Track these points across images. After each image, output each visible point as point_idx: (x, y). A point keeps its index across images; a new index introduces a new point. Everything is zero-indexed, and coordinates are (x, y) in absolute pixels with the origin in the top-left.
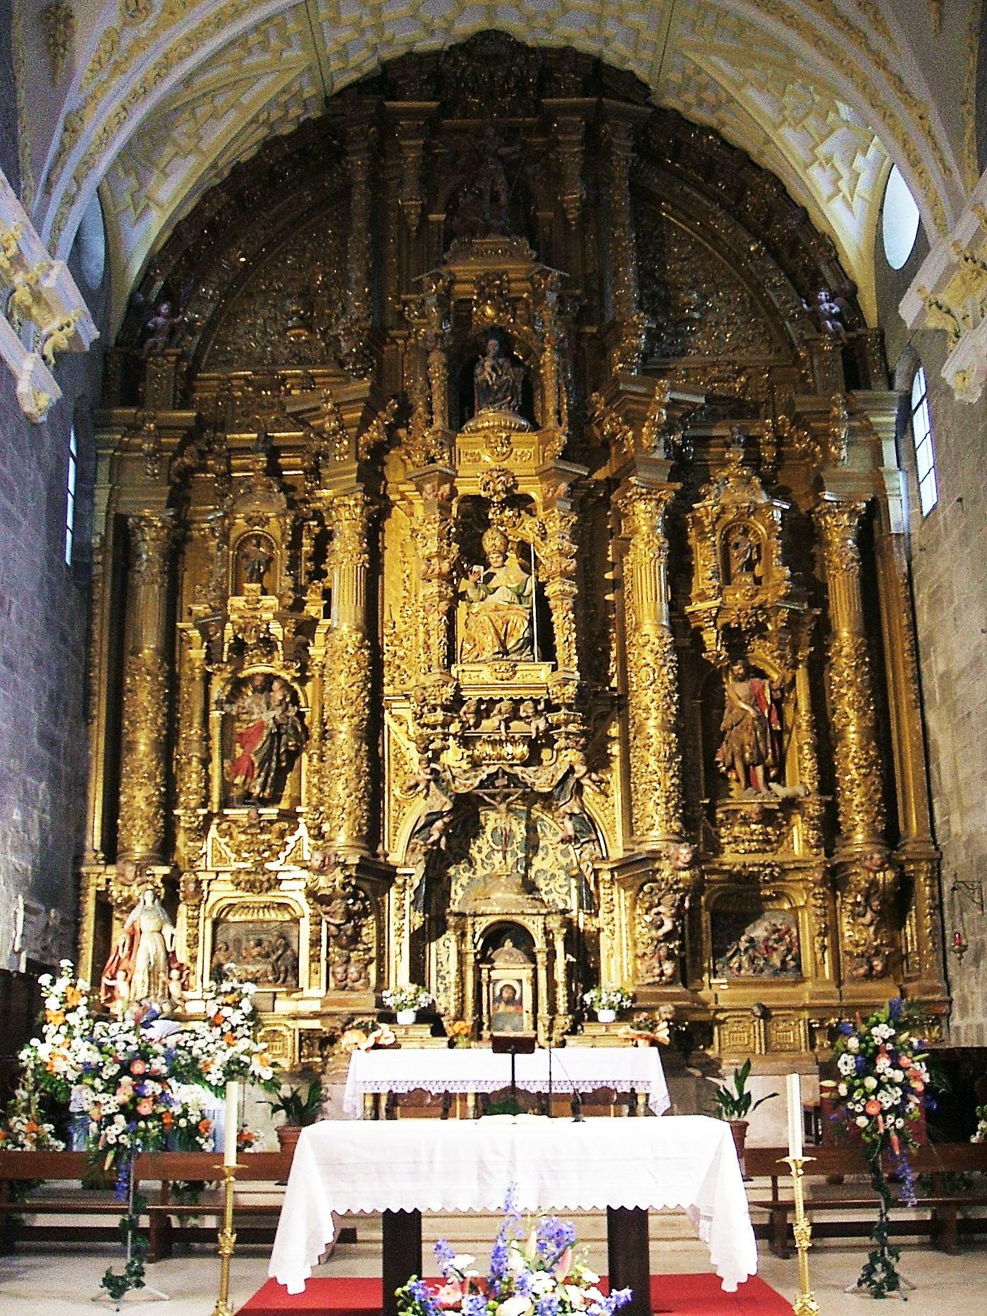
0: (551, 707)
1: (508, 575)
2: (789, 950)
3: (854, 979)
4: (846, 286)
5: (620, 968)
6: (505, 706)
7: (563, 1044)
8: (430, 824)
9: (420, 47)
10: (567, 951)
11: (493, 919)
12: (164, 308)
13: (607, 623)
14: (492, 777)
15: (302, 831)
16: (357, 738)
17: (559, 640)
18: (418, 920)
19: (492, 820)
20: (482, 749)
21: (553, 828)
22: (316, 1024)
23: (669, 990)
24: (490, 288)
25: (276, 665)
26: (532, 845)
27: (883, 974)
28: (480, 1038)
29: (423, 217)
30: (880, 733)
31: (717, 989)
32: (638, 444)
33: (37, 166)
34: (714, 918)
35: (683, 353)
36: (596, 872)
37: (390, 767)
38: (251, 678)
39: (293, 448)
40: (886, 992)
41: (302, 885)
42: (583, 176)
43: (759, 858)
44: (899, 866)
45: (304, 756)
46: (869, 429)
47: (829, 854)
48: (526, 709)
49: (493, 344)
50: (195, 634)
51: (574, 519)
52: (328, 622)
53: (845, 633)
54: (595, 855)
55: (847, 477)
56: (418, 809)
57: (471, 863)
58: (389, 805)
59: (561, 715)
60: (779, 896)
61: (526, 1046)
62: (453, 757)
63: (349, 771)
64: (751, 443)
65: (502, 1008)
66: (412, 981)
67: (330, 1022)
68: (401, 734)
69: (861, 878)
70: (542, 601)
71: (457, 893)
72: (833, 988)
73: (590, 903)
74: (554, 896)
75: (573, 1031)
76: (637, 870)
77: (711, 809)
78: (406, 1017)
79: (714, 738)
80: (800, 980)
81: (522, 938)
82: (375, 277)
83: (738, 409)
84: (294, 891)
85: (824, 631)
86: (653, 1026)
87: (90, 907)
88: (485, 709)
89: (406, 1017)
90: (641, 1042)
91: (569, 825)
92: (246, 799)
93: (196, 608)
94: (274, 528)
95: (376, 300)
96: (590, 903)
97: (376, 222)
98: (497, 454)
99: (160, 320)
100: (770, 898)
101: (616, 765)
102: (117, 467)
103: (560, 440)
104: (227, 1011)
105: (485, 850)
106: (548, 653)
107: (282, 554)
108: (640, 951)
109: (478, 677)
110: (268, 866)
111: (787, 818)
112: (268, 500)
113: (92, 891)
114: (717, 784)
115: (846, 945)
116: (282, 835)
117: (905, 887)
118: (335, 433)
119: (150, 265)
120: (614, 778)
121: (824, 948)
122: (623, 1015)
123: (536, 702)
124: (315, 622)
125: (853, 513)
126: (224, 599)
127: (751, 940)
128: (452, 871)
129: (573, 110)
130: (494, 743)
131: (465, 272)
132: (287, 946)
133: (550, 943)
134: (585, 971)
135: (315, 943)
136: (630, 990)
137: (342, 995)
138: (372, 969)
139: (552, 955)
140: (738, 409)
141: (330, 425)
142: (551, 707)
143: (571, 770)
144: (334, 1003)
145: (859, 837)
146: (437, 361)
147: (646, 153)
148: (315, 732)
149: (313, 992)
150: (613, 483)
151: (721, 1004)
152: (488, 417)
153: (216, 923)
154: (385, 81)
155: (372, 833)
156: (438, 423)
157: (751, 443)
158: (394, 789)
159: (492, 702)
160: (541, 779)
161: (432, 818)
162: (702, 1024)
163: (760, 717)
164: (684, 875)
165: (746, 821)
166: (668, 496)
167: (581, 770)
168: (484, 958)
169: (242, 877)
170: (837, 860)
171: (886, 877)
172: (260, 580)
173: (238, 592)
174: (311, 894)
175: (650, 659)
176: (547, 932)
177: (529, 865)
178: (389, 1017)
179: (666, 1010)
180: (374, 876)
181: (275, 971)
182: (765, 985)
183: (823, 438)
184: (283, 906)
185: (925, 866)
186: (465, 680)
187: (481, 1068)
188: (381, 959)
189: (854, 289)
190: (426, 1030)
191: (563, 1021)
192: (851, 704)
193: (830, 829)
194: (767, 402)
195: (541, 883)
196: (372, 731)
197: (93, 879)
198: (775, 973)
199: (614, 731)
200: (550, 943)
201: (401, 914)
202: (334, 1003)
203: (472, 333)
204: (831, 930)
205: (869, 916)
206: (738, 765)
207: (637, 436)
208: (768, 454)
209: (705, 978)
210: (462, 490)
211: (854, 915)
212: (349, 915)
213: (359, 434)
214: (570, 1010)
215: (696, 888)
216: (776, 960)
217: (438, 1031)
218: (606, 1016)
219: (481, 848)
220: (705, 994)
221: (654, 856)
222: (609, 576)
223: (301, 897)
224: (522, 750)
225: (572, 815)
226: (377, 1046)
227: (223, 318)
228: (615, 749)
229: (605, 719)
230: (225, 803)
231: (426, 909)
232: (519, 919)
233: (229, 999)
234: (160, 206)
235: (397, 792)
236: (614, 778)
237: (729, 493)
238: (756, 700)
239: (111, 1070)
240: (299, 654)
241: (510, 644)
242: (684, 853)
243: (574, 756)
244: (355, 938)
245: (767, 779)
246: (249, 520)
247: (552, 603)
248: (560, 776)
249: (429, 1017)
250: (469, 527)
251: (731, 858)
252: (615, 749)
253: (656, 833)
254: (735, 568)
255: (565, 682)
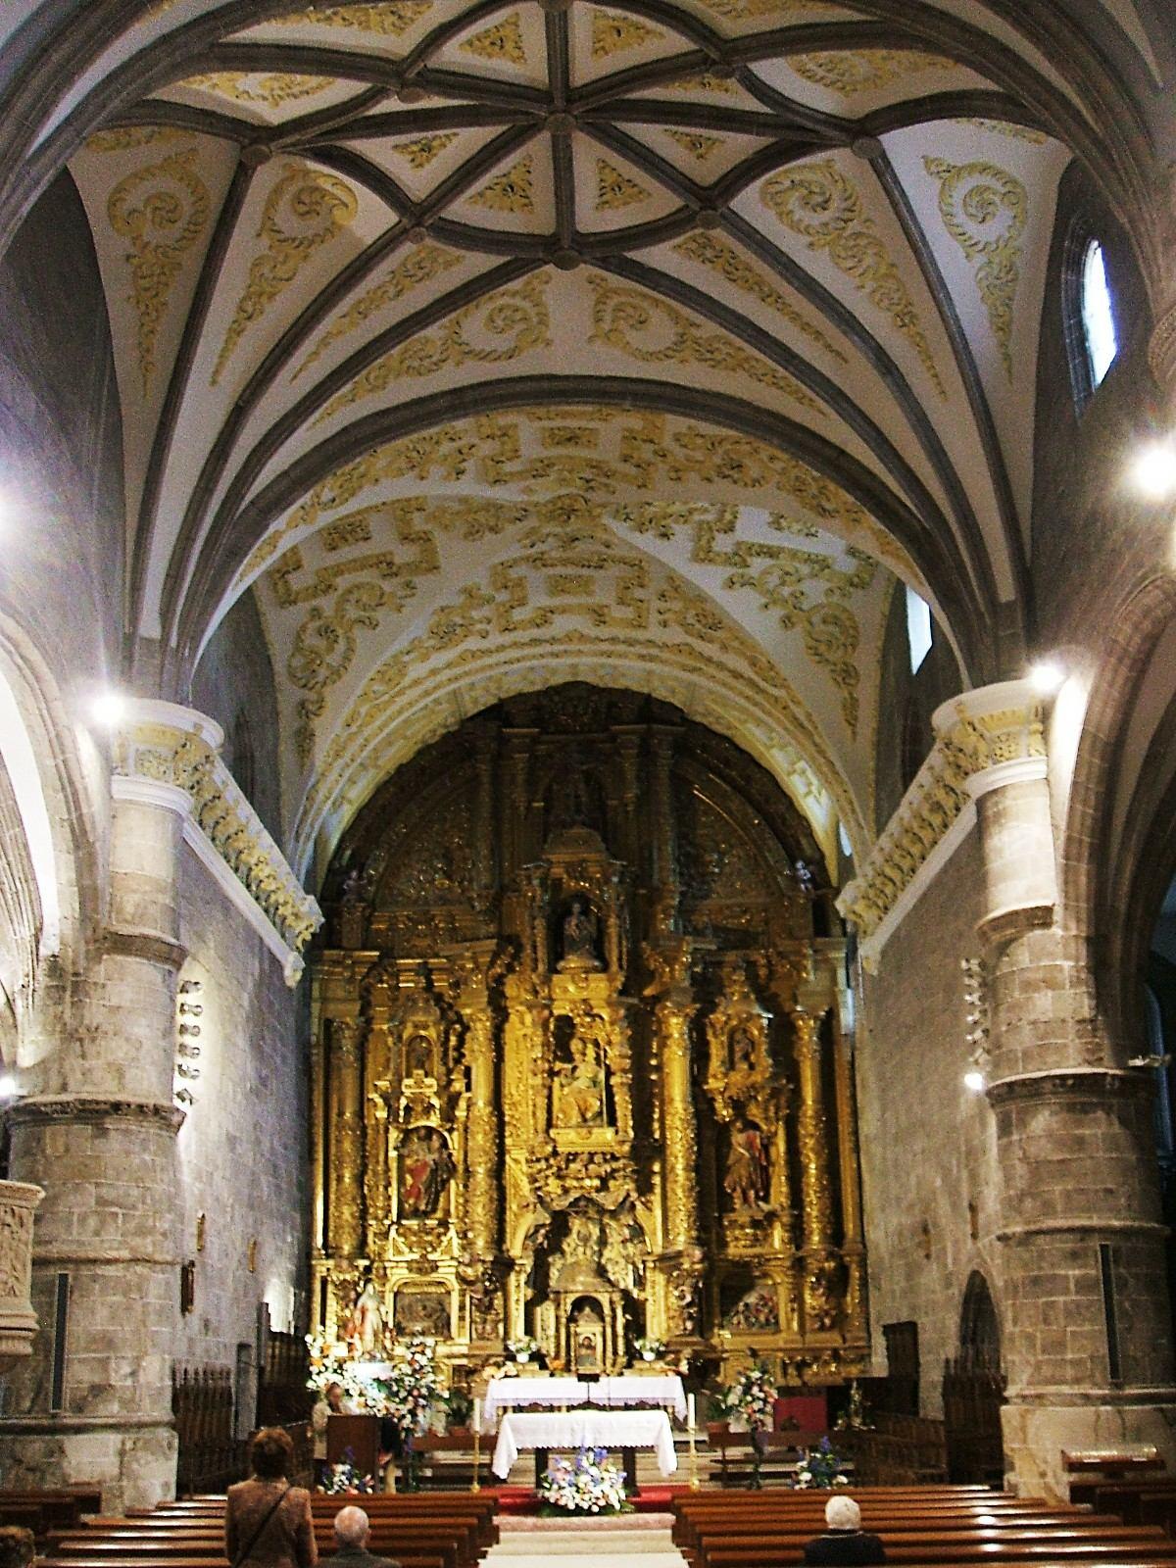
0: (614, 1158)
1: (587, 1069)
2: (771, 1311)
3: (813, 1331)
4: (817, 856)
5: (659, 1325)
6: (585, 1157)
7: (621, 1374)
8: (536, 1231)
9: (526, 690)
10: (624, 1313)
11: (578, 1295)
12: (354, 874)
13: (652, 1095)
14: (577, 1200)
15: (452, 1233)
16: (489, 1176)
17: (619, 1114)
18: (530, 1293)
19: (576, 1224)
20: (569, 1183)
21: (617, 1232)
22: (464, 1361)
23: (690, 1339)
24: (577, 870)
25: (434, 1121)
26: (603, 1242)
27: (832, 1327)
28: (569, 1371)
29: (529, 808)
30: (831, 1170)
31: (724, 1337)
32: (672, 977)
33: (291, 823)
34: (719, 1290)
35: (707, 896)
36: (644, 1262)
37: (510, 1191)
38: (417, 1129)
39: (441, 970)
40: (833, 1339)
41: (454, 1270)
42: (638, 778)
43: (751, 1251)
44: (839, 1259)
45: (452, 1182)
46: (827, 961)
47: (798, 1248)
48: (597, 1159)
49: (576, 907)
50: (380, 1101)
51: (630, 1033)
52: (469, 1095)
53: (810, 1102)
54: (647, 1248)
55: (813, 993)
56: (527, 1222)
57: (563, 1253)
58: (509, 1216)
59: (620, 1164)
60: (765, 1275)
61: (595, 1378)
62: (553, 1186)
63: (484, 1199)
64: (751, 967)
65: (584, 1351)
66: (526, 1333)
67: (474, 1361)
68: (517, 1170)
69: (813, 1265)
70: (609, 1088)
71: (554, 1273)
72: (798, 1337)
73: (640, 1282)
74: (618, 1276)
75: (629, 1365)
76: (668, 1262)
77: (720, 1219)
78: (523, 1358)
79: (723, 1170)
80: (778, 1331)
81: (596, 1306)
82: (495, 852)
83: (744, 939)
84: (447, 1273)
85: (796, 1097)
86: (676, 1362)
87: (317, 1286)
88: (572, 1157)
89: (523, 1358)
90: (670, 1373)
91: (626, 1232)
92: (416, 1213)
93: (378, 1083)
94: (432, 1033)
95: (497, 869)
96: (640, 1282)
97: (496, 815)
98: (583, 990)
99: (351, 882)
100: (759, 1277)
101: (658, 1190)
102: (324, 984)
103: (620, 979)
104: (418, 1357)
105: (573, 1245)
106: (612, 1121)
107: (437, 1051)
108: (672, 1313)
109: (568, 1138)
110: (431, 1257)
111: (771, 1225)
112: (426, 1011)
113: (318, 1275)
114: (725, 1204)
115: (808, 1309)
116: (439, 1236)
117: (843, 1271)
118: (473, 970)
119: (342, 840)
120: (656, 1198)
121: (793, 1310)
122: (660, 1355)
123: (604, 1154)
124: (459, 1094)
125: (816, 1018)
126: (400, 1081)
127: (746, 1305)
128: (550, 1259)
129: (633, 732)
130: (578, 1179)
131: (559, 860)
132: (443, 1310)
133: (613, 1310)
134: (637, 1328)
135: (462, 1308)
136: (665, 1340)
137: (481, 1343)
138: (501, 1327)
139: (614, 1318)
140: (744, 939)
141: (470, 966)
142: (614, 1158)
143: (628, 1195)
144: (478, 1348)
145: (816, 1238)
146: (540, 923)
147: (681, 748)
148: (461, 1168)
149: (461, 1341)
150: (657, 999)
151: (726, 1347)
152: (573, 962)
153: (396, 1295)
154: (499, 713)
155: (499, 1239)
156: (541, 968)
157: (751, 967)
158: (513, 1206)
159: (576, 1155)
160: (608, 1201)
161: (538, 1228)
162: (711, 1360)
163: (753, 1157)
164: (698, 1266)
165: (742, 1227)
166: (691, 1011)
167: (634, 1195)
168: (572, 1319)
169: (415, 1265)
170: (800, 1254)
171: (830, 1265)
172: (422, 1067)
173: (409, 1075)
174: (462, 1279)
175: (678, 1123)
176: (611, 1302)
177: (601, 1255)
178: (511, 1357)
179: (687, 1352)
180: (503, 1265)
181: (436, 1327)
182: (754, 1334)
183: (798, 967)
184: (440, 1283)
185: (855, 1258)
186: (559, 1139)
187: (568, 1388)
188: (506, 1320)
189: (823, 856)
190: (536, 1366)
191: (622, 1360)
192: (812, 1149)
193: (797, 1233)
194: (763, 933)
195: (609, 1267)
196: (498, 1171)
197: (318, 1268)
198: (762, 1327)
199: (656, 1167)
200: (613, 1310)
201: (519, 1289)
202: (478, 1348)
203: (562, 896)
204: (798, 1299)
205: (821, 1290)
206: (739, 1190)
207: (672, 970)
208: (763, 972)
209: (716, 1330)
210: (556, 1012)
211: (813, 1289)
212: (487, 1292)
213: (489, 969)
214: (626, 1353)
215: (706, 1275)
216: (762, 1318)
217: (543, 1366)
218: (649, 1356)
219: (570, 1243)
220: (715, 1341)
221: (679, 1254)
222: (653, 1062)
223: (453, 1278)
224: (596, 1182)
225: (629, 1226)
226: (506, 1376)
227: (393, 871)
228: (657, 1180)
229: (650, 1160)
230: (400, 1216)
231: (534, 1287)
232: (594, 1295)
233: (419, 1349)
234: (350, 802)
235: (514, 1207)
236: (656, 1198)
237: (737, 1007)
238: (750, 1146)
239: (403, 1394)
240: (448, 1116)
241: (589, 1115)
242: (698, 1253)
243: (630, 1186)
244: (490, 1307)
245: (757, 1197)
246: (416, 1026)
247: (615, 1089)
248: (621, 1199)
249: (538, 1357)
250: (561, 1037)
251: (734, 1250)
252: (657, 1180)
253: (682, 1238)
254: (738, 1055)
255: (623, 1142)
